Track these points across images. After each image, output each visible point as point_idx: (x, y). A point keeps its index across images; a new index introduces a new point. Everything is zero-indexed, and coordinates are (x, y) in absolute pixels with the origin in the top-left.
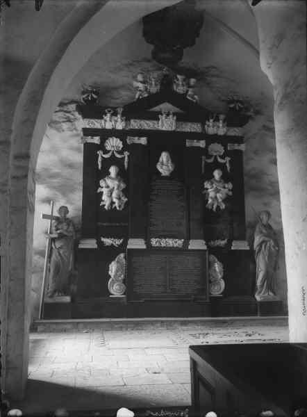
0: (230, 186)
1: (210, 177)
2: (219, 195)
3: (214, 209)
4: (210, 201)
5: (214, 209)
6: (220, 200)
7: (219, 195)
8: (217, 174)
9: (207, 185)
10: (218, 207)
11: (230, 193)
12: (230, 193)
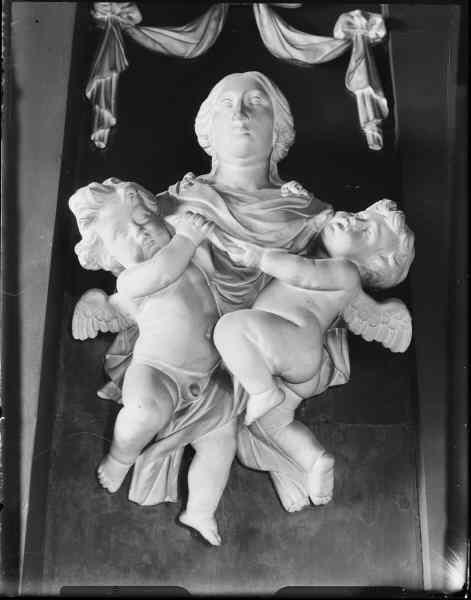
0: (381, 234)
1: (161, 156)
2: (241, 342)
3: (200, 515)
5: (200, 515)
6: (260, 400)
7: (241, 342)
8: (230, 123)
9: (107, 222)
10: (249, 487)
11: (394, 328)
12: (394, 328)
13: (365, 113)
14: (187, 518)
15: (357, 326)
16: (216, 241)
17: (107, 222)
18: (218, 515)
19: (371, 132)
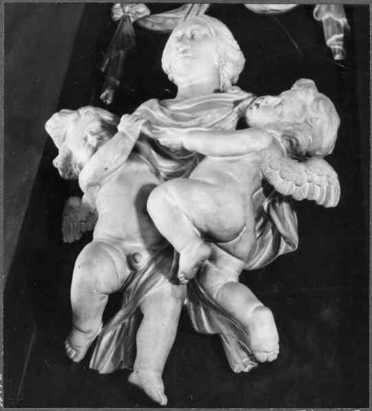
0: (308, 111)
3: (149, 374)
4: (91, 278)
5: (149, 374)
9: (72, 132)
10: (196, 352)
13: (327, 30)
14: (133, 378)
15: (283, 186)
16: (147, 132)
17: (72, 132)
18: (168, 374)
19: (334, 41)
